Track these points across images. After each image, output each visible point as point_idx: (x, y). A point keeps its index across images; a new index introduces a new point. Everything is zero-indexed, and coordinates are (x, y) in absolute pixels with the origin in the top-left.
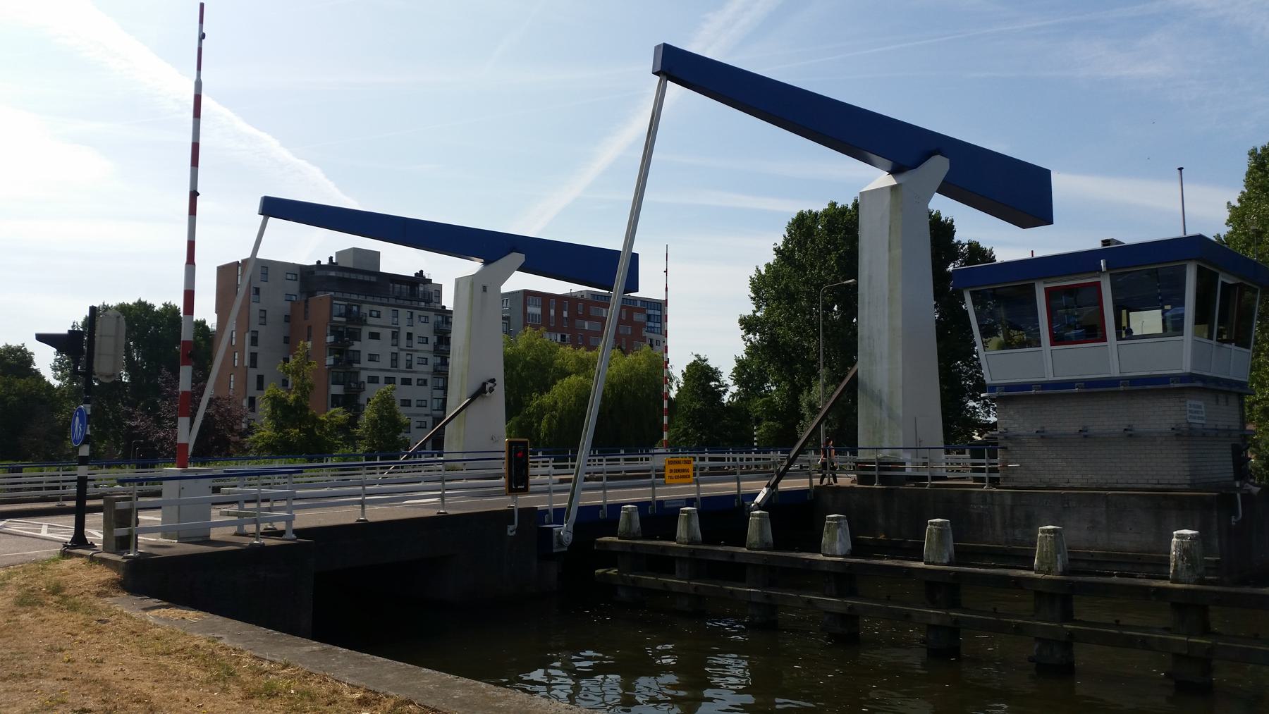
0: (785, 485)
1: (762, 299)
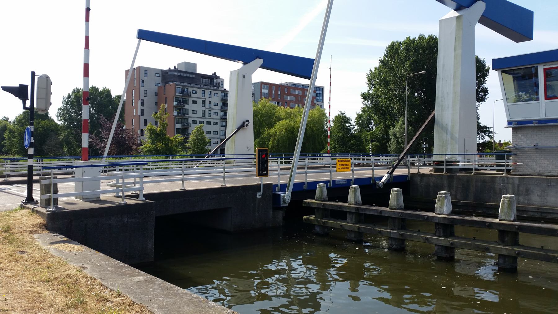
0: (397, 172)
1: (372, 84)
